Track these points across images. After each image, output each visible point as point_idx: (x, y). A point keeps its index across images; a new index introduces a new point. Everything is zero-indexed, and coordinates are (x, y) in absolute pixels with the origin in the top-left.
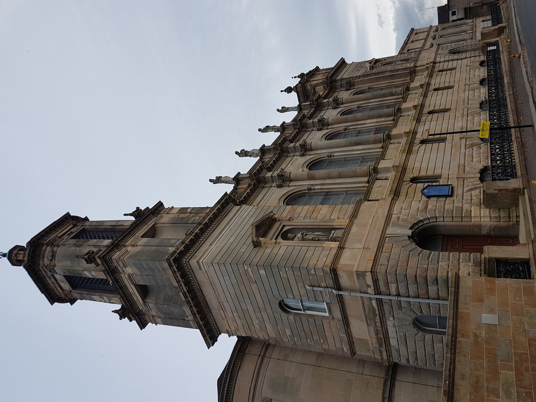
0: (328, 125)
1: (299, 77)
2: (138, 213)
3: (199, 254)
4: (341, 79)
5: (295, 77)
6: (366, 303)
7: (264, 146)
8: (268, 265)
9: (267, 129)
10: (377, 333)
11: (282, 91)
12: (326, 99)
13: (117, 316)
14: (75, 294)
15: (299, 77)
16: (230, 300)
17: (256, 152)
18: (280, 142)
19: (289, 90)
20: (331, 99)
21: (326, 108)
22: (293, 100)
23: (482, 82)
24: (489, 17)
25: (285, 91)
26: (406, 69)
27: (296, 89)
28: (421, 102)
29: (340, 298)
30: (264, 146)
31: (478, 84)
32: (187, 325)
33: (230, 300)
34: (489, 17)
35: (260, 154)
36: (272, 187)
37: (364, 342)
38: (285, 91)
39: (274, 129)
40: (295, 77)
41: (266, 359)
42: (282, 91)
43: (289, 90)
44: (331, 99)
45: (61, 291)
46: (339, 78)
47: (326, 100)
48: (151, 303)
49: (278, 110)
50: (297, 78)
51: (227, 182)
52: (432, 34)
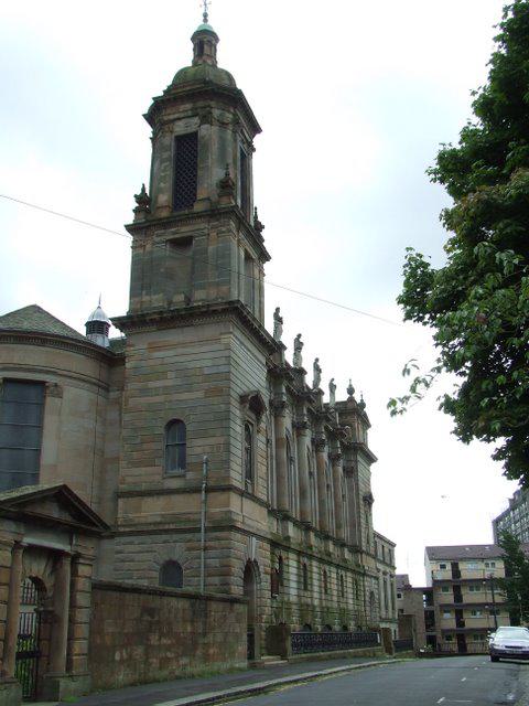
0: (333, 466)
1: (362, 400)
2: (259, 227)
3: (238, 333)
4: (356, 461)
6: (196, 517)
8: (226, 418)
10: (155, 524)
13: (139, 192)
14: (168, 140)
15: (362, 400)
16: (177, 359)
19: (351, 391)
20: (306, 419)
22: (341, 396)
23: (308, 626)
24: (397, 638)
26: (360, 541)
27: (351, 400)
28: (292, 547)
29: (197, 490)
31: (327, 622)
32: (135, 291)
33: (177, 359)
34: (397, 638)
37: (138, 509)
41: (96, 388)
43: (351, 391)
44: (285, 398)
45: (172, 117)
46: (359, 458)
48: (167, 250)
49: (299, 336)
52: (388, 570)
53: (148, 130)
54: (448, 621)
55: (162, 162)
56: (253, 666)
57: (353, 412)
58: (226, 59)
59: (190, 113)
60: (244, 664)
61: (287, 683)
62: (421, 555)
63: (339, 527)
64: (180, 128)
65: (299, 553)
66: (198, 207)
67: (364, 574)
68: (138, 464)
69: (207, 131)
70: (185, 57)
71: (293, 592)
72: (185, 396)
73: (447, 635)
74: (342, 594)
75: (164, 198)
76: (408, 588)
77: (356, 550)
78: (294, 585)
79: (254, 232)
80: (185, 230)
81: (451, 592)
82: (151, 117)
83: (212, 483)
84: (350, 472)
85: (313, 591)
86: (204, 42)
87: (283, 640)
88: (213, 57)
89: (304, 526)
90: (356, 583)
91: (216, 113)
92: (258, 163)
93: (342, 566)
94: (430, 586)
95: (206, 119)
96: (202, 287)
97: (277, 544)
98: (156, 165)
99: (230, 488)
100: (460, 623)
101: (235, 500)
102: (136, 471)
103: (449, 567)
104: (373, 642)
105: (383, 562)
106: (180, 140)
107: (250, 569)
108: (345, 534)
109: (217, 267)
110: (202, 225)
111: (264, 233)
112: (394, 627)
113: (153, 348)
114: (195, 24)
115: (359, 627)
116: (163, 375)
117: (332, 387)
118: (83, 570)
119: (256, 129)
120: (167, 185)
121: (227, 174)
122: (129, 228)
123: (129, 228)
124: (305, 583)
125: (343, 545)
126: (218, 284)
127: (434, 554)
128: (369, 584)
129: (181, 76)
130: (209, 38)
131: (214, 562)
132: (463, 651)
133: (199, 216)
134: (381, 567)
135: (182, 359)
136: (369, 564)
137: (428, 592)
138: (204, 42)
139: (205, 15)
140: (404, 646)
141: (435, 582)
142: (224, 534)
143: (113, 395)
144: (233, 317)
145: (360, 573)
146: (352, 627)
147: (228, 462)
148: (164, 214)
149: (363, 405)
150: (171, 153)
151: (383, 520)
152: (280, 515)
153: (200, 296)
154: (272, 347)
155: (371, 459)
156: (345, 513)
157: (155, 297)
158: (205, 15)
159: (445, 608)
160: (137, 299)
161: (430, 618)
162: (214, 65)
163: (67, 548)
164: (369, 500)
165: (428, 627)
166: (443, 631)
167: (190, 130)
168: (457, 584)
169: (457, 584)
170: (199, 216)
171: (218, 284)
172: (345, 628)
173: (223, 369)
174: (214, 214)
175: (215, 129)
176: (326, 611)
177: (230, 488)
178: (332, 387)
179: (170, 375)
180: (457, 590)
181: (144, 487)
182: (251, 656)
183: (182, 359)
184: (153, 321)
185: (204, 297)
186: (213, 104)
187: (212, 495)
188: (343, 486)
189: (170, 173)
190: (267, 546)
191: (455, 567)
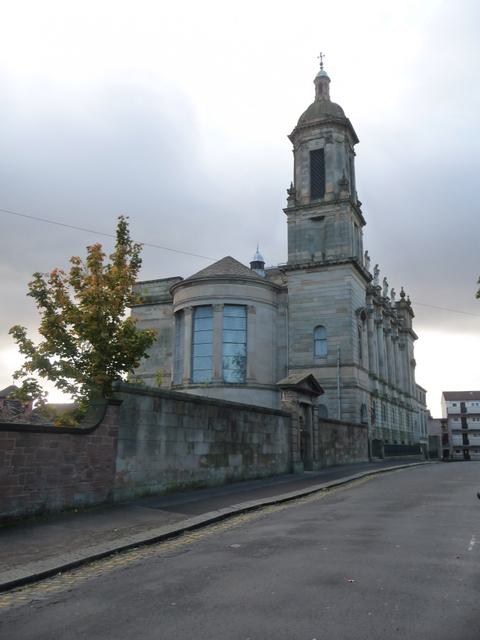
4: (407, 340)
14: (306, 154)
19: (403, 295)
22: (398, 298)
32: (290, 250)
43: (403, 295)
53: (290, 146)
54: (458, 440)
55: (302, 168)
56: (371, 461)
57: (405, 307)
58: (335, 96)
59: (318, 136)
60: (367, 460)
61: (244, 511)
62: (439, 397)
63: (398, 382)
64: (313, 146)
65: (382, 399)
66: (327, 198)
67: (412, 411)
68: (299, 350)
69: (329, 149)
70: (309, 97)
71: (380, 422)
72: (324, 312)
73: (457, 449)
74: (401, 424)
75: (305, 192)
76: (430, 418)
77: (407, 395)
78: (380, 418)
79: (356, 207)
80: (319, 212)
81: (460, 421)
82: (292, 138)
83: (343, 362)
84: (403, 347)
85: (391, 421)
86: (322, 83)
87: (380, 448)
88: (327, 94)
89: (382, 382)
90: (407, 415)
91: (335, 135)
92: (359, 163)
93: (401, 405)
94: (446, 417)
95: (329, 140)
96: (332, 247)
97: (374, 394)
98: (298, 170)
99: (353, 365)
100: (466, 441)
101: (355, 369)
102: (297, 354)
103: (458, 404)
104: (419, 453)
105: (420, 403)
106: (313, 153)
107: (363, 407)
108: (401, 386)
109: (341, 235)
110: (329, 209)
111: (362, 208)
112: (427, 442)
113: (304, 283)
114: (315, 72)
115: (410, 442)
116: (311, 300)
117: (393, 294)
118: (316, 413)
119: (356, 141)
120: (307, 183)
121: (344, 176)
122: (286, 211)
123: (286, 211)
124: (384, 417)
125: (393, 389)
126: (341, 246)
127: (449, 396)
128: (414, 416)
129: (311, 109)
130: (324, 81)
131: (345, 406)
132: (467, 458)
133: (328, 203)
134: (419, 405)
135: (322, 290)
136: (414, 403)
137: (443, 421)
138: (322, 83)
139: (321, 64)
140: (433, 455)
141: (449, 415)
142: (351, 390)
143: (281, 310)
144: (351, 266)
145: (410, 409)
146: (406, 443)
147: (352, 350)
148: (306, 202)
149: (409, 303)
150: (307, 162)
151: (421, 377)
152: (373, 377)
153: (331, 253)
154: (367, 278)
155: (415, 337)
156: (401, 373)
157: (303, 253)
158: (321, 64)
159: (456, 432)
160: (293, 254)
161: (446, 438)
162: (329, 100)
163: (309, 402)
164: (413, 363)
165: (444, 444)
166: (455, 447)
167: (320, 147)
168: (464, 416)
169: (464, 416)
170: (328, 203)
171: (341, 246)
172: (403, 442)
173: (348, 297)
174: (337, 201)
175: (334, 146)
176: (394, 432)
177: (353, 365)
178: (393, 294)
179: (315, 300)
180: (464, 420)
181: (303, 364)
182: (369, 456)
183: (322, 290)
184: (304, 268)
185: (333, 254)
186: (332, 129)
187: (343, 368)
188: (399, 353)
189: (307, 176)
190: (369, 396)
191: (463, 405)
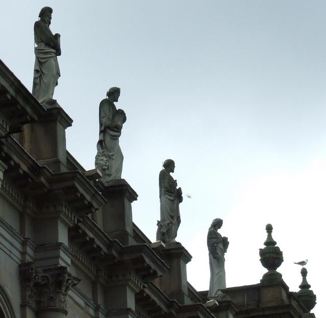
1: (305, 286)
5: (304, 273)
7: (68, 122)
9: (171, 192)
11: (269, 229)
12: (71, 239)
15: (305, 286)
17: (114, 164)
18: (147, 261)
19: (271, 256)
20: (65, 260)
21: (100, 301)
22: (243, 271)
25: (270, 243)
27: (273, 281)
30: (68, 122)
35: (106, 180)
36: (24, 244)
38: (270, 243)
39: (170, 220)
40: (304, 273)
42: (269, 229)
43: (271, 256)
47: (63, 237)
50: (300, 280)
51: (39, 73)
